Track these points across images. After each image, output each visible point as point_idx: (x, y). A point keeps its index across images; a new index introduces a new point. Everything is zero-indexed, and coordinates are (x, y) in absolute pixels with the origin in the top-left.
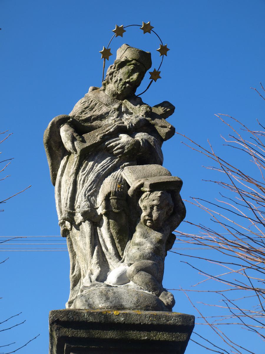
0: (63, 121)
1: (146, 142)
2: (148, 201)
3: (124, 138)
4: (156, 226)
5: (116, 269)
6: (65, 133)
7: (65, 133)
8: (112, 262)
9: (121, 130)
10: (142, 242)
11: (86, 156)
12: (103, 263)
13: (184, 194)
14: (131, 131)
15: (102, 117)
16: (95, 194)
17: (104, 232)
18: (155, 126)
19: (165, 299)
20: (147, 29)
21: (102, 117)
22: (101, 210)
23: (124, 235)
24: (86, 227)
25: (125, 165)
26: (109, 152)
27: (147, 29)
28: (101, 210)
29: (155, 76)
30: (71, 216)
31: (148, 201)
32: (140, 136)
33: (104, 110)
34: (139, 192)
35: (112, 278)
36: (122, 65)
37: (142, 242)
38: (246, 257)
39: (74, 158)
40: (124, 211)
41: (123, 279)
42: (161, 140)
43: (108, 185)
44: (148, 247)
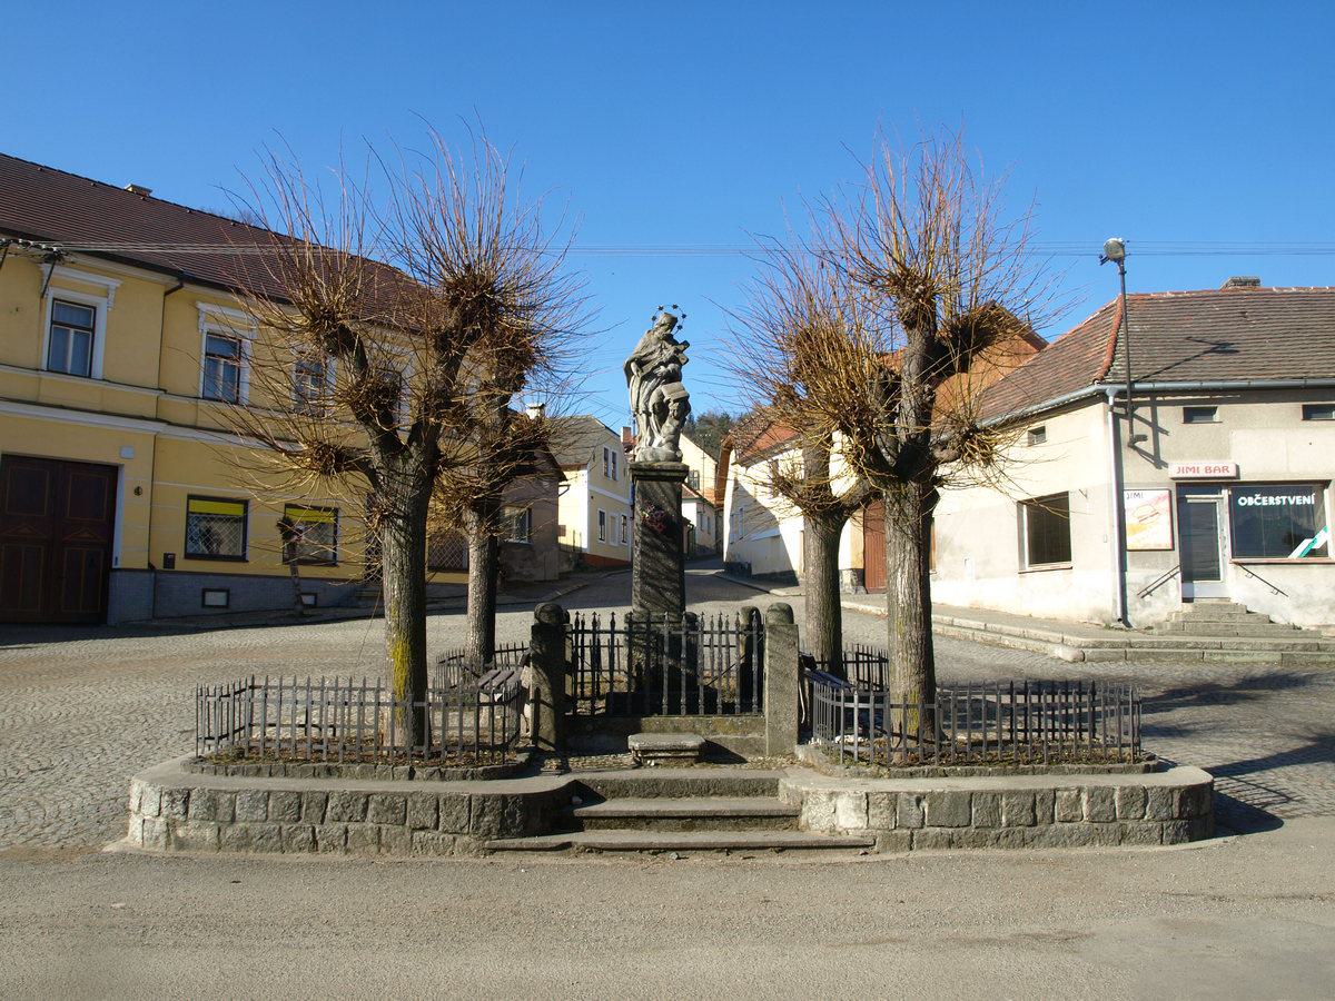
0: (633, 361)
1: (674, 370)
2: (673, 407)
3: (662, 368)
4: (676, 418)
5: (659, 439)
6: (633, 366)
7: (633, 366)
8: (656, 434)
9: (661, 364)
10: (669, 426)
11: (644, 379)
12: (652, 434)
13: (690, 400)
14: (666, 365)
15: (652, 353)
16: (648, 401)
17: (652, 418)
18: (622, 688)
19: (679, 455)
20: (675, 307)
21: (652, 353)
22: (651, 410)
23: (661, 421)
24: (644, 416)
25: (666, 366)
26: (655, 376)
27: (675, 307)
28: (651, 410)
29: (680, 327)
30: (637, 410)
31: (673, 407)
32: (671, 367)
33: (653, 348)
34: (668, 401)
35: (655, 445)
36: (662, 325)
37: (669, 426)
38: (712, 622)
39: (638, 379)
40: (661, 410)
41: (660, 445)
42: (681, 365)
43: (654, 399)
44: (672, 429)
